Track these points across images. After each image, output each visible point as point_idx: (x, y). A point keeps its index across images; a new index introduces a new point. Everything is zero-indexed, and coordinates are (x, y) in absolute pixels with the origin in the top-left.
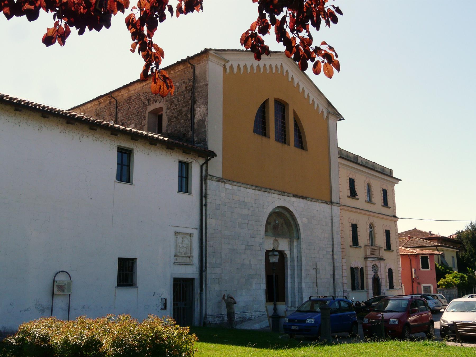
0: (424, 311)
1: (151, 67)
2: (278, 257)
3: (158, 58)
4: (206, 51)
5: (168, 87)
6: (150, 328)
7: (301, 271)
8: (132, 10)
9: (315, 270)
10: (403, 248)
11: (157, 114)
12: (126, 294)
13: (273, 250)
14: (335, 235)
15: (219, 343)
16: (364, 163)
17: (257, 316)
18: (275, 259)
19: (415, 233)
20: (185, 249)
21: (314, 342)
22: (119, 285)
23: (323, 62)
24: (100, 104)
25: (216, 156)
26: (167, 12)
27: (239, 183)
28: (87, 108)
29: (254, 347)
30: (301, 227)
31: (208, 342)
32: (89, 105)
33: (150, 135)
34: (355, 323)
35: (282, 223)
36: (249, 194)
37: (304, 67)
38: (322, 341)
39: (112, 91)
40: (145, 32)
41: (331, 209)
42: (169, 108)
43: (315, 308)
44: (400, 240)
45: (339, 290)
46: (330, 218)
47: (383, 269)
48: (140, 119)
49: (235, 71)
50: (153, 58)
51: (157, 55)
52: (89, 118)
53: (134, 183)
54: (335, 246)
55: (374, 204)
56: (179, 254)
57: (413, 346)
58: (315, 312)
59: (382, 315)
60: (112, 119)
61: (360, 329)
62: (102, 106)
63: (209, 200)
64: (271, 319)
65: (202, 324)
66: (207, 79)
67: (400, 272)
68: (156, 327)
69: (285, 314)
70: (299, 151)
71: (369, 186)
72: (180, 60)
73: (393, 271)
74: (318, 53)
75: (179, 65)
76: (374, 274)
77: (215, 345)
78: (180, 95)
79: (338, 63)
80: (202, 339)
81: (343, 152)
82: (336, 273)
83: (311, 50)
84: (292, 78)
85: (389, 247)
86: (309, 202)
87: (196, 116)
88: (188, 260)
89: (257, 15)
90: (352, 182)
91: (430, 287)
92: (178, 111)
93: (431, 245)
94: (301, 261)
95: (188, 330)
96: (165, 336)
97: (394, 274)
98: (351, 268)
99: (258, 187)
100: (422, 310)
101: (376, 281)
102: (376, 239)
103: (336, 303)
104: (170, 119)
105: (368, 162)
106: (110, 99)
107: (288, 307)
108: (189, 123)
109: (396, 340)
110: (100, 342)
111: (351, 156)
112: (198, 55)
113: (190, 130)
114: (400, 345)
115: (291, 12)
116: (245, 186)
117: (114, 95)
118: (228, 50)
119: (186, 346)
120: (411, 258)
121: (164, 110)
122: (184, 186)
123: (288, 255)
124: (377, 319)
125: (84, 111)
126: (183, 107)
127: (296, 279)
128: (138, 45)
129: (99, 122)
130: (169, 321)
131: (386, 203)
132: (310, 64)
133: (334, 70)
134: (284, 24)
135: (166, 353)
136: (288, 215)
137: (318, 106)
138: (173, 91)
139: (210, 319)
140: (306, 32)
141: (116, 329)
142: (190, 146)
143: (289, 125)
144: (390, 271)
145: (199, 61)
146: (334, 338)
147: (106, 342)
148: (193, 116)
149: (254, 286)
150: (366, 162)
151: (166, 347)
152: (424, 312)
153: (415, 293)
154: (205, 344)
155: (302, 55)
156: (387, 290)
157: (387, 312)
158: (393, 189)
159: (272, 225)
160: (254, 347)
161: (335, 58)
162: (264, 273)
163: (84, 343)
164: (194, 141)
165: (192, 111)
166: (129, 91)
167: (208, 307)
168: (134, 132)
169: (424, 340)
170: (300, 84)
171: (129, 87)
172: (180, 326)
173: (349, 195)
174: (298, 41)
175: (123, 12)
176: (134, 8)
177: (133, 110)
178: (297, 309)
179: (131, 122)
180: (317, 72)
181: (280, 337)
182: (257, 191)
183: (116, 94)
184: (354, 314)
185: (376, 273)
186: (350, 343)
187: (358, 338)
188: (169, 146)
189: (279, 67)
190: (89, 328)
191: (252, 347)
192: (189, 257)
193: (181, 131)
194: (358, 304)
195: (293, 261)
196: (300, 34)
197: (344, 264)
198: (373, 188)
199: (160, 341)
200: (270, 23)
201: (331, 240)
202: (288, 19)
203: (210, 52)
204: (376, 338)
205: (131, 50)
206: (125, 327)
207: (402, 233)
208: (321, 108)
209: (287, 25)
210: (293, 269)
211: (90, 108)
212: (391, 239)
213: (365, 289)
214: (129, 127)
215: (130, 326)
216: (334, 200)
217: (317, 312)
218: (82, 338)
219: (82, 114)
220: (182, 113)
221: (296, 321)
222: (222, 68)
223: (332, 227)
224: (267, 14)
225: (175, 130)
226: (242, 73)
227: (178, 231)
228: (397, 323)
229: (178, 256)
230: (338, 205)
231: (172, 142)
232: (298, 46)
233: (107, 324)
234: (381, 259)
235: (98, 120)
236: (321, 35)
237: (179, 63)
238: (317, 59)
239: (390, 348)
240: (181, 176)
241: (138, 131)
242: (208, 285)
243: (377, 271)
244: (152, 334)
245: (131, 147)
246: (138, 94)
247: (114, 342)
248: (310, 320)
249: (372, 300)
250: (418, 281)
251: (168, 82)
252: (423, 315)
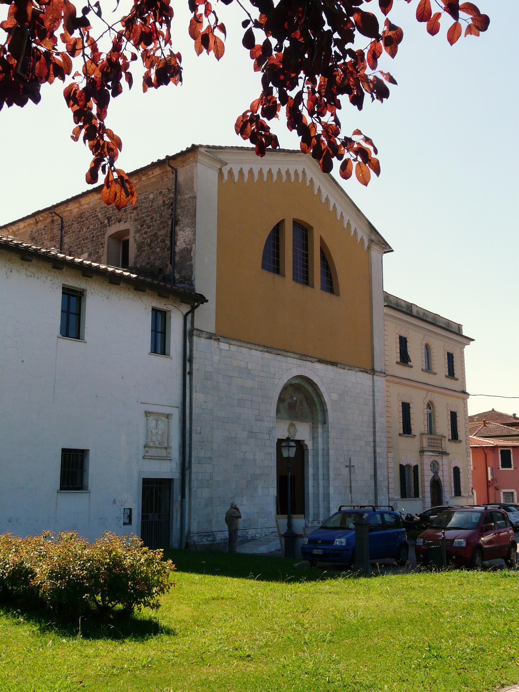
0: (505, 528)
1: (103, 163)
2: (294, 449)
3: (112, 150)
4: (194, 149)
5: (127, 194)
6: (106, 551)
7: (328, 470)
8: (73, 78)
9: (348, 469)
10: (475, 438)
11: (121, 240)
12: (73, 500)
13: (288, 440)
14: (378, 418)
15: (208, 574)
16: (421, 314)
17: (264, 535)
18: (290, 453)
19: (492, 416)
20: (159, 438)
21: (344, 573)
22: (62, 488)
23: (355, 160)
24: (37, 223)
25: (207, 301)
26: (123, 81)
27: (240, 341)
28: (19, 229)
29: (257, 580)
30: (329, 406)
31: (192, 572)
32: (22, 225)
33: (110, 269)
34: (405, 545)
35: (302, 400)
36: (254, 358)
37: (327, 168)
38: (357, 571)
39: (55, 204)
40: (94, 111)
41: (373, 380)
42: (138, 231)
43: (347, 523)
44: (471, 425)
45: (382, 498)
46: (371, 394)
47: (446, 468)
48: (96, 246)
49: (236, 178)
50: (106, 150)
51: (112, 146)
52: (11, 241)
53: (86, 338)
54: (378, 434)
55: (435, 374)
56: (151, 444)
57: (487, 578)
58: (348, 529)
59: (444, 533)
60: (55, 246)
61: (412, 554)
62: (40, 226)
63: (195, 366)
64: (283, 539)
65: (183, 547)
66: (195, 190)
67: (470, 472)
68: (114, 549)
69: (305, 532)
70: (327, 295)
71: (427, 347)
72: (155, 161)
73: (461, 470)
74: (349, 146)
75: (155, 168)
76: (433, 474)
77: (201, 576)
79: (378, 162)
80: (181, 567)
81: (391, 298)
82: (378, 473)
83: (339, 143)
84: (319, 190)
85: (455, 436)
86: (341, 371)
87: (178, 244)
88: (164, 453)
89: (259, 89)
90: (403, 342)
91: (512, 493)
92: (151, 236)
93: (515, 433)
94: (328, 455)
95: (161, 554)
96: (127, 562)
97: (461, 475)
98: (401, 466)
99: (268, 348)
100: (500, 527)
101: (436, 485)
102: (437, 425)
103: (378, 516)
104: (140, 247)
105: (426, 313)
106: (53, 217)
107: (308, 521)
108: (167, 253)
109: (462, 570)
110: (32, 572)
111: (403, 304)
112: (182, 153)
113: (168, 263)
114: (468, 576)
115: (310, 86)
116: (249, 346)
117: (58, 211)
118: (226, 148)
119: (158, 578)
120: (488, 452)
121: (132, 233)
122: (159, 345)
123: (310, 447)
124: (436, 539)
125: (14, 234)
126: (159, 229)
127: (321, 482)
128: (83, 131)
129: (34, 250)
130: (133, 541)
131: (451, 373)
132: (337, 163)
133: (372, 173)
134: (300, 104)
135: (128, 587)
136: (310, 389)
137: (355, 232)
138: (134, 199)
139: (195, 539)
140: (332, 115)
141: (56, 552)
142: (169, 286)
143: (314, 258)
144: (456, 471)
145: (183, 162)
146: (374, 566)
147: (41, 572)
148: (173, 243)
149: (260, 491)
150: (424, 314)
151: (129, 579)
152: (503, 530)
153: (492, 502)
154: (186, 575)
155: (323, 149)
156: (451, 498)
157: (450, 529)
158: (462, 353)
159: (286, 404)
160: (258, 579)
161: (373, 155)
162: (274, 472)
163: (9, 573)
164: (174, 280)
165: (173, 236)
166: (81, 205)
167: (192, 521)
168: (87, 265)
169: (501, 570)
170: (330, 198)
171: (81, 200)
172: (149, 549)
173: (399, 360)
174: (320, 129)
175: (63, 79)
176: (77, 74)
177: (85, 233)
178: (321, 525)
179: (82, 250)
180: (345, 173)
181: (296, 565)
182: (266, 354)
183: (62, 208)
184: (403, 532)
185: (436, 473)
186: (397, 574)
187: (408, 565)
188: (138, 287)
189: (300, 173)
190: (16, 551)
191: (254, 579)
192: (166, 448)
193: (156, 264)
194: (410, 518)
195: (316, 455)
196: (323, 119)
197: (390, 460)
198: (433, 350)
199: (121, 570)
200: (278, 102)
201: (371, 425)
202: (305, 96)
203: (200, 149)
204: (434, 567)
205: (72, 137)
206: (68, 550)
207: (474, 416)
208: (360, 234)
209: (304, 105)
210: (316, 467)
211: (23, 228)
212: (459, 424)
213: (420, 496)
214: (80, 258)
215: (77, 547)
216: (377, 367)
217: (351, 529)
218: (6, 565)
219: (11, 238)
220: (158, 238)
221: (320, 542)
222: (216, 174)
223: (374, 406)
224: (274, 88)
225: (147, 263)
226: (245, 181)
227: (150, 410)
228: (464, 545)
229: (149, 447)
230: (382, 375)
231: (142, 280)
232: (319, 135)
233: (42, 545)
234: (444, 453)
235: (34, 247)
236: (351, 118)
237: (154, 165)
238: (348, 155)
239: (454, 581)
240: (154, 331)
241: (93, 264)
242: (193, 489)
243: (438, 470)
244: (108, 560)
245: (83, 287)
246: (94, 209)
247: (52, 571)
248: (340, 540)
249: (430, 512)
250: (495, 485)
251: (128, 186)
252: (501, 534)
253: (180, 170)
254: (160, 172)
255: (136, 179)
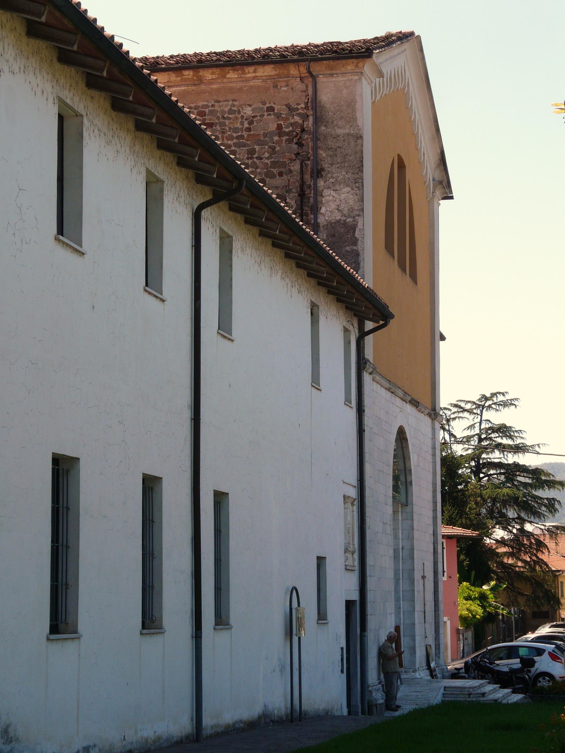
12: (65, 652)
78: (262, 143)
87: (323, 210)
94: (412, 558)
253: (321, 79)
254: (274, 73)
255: (213, 73)
